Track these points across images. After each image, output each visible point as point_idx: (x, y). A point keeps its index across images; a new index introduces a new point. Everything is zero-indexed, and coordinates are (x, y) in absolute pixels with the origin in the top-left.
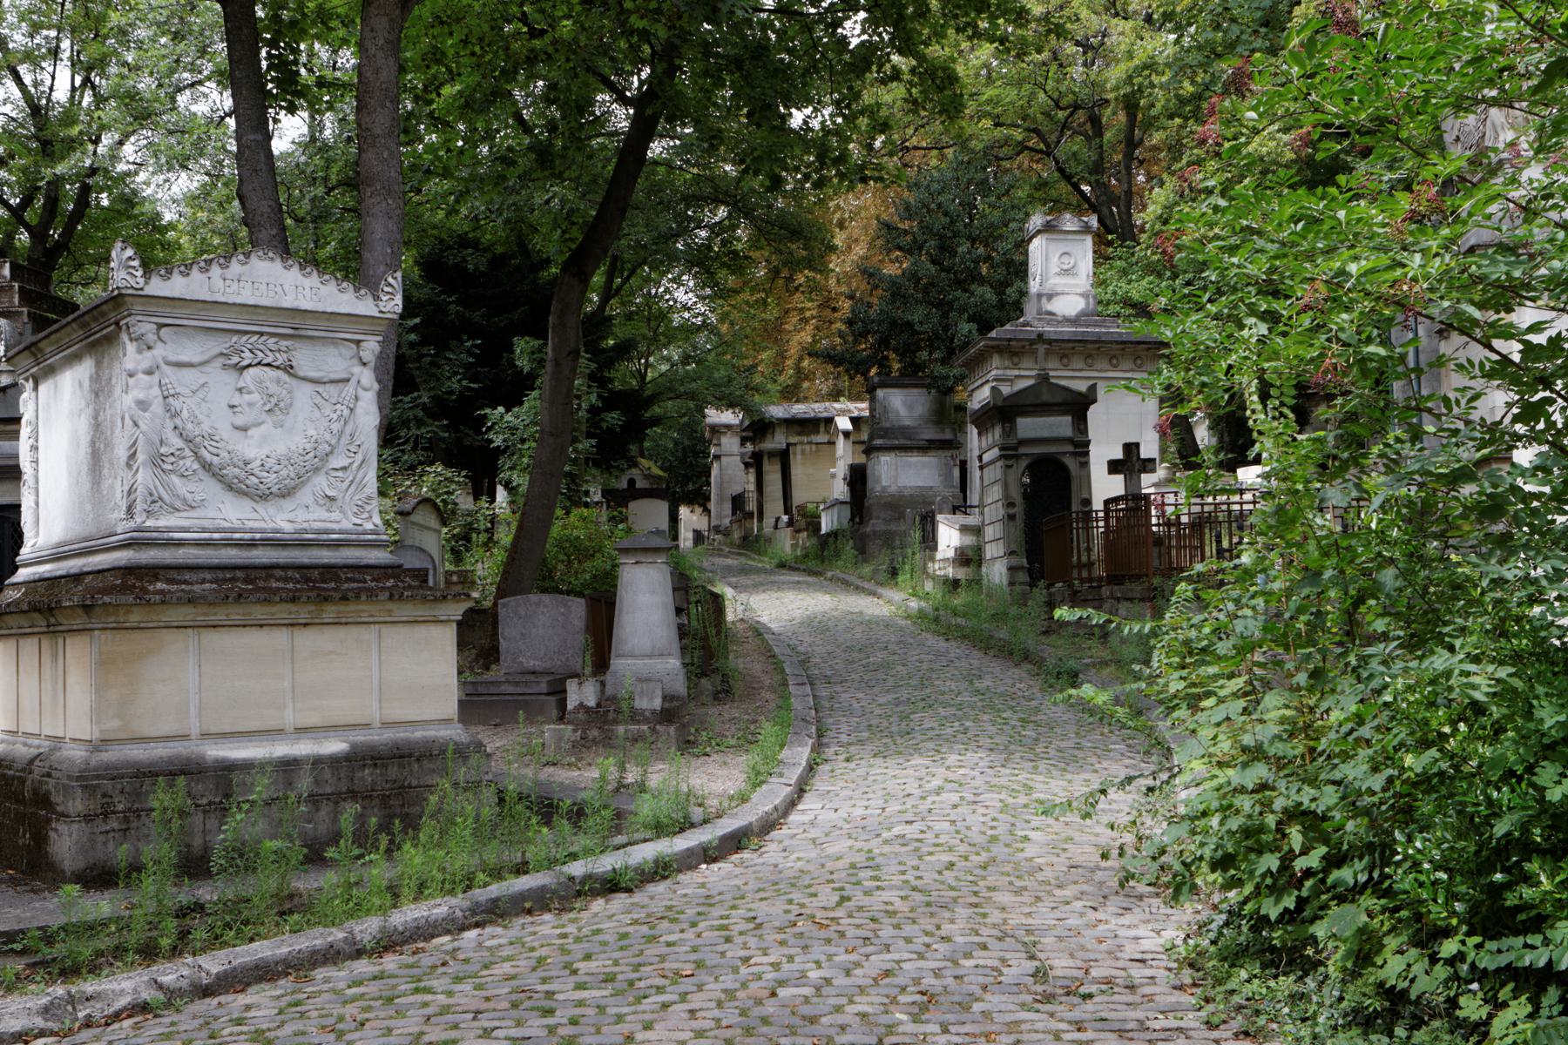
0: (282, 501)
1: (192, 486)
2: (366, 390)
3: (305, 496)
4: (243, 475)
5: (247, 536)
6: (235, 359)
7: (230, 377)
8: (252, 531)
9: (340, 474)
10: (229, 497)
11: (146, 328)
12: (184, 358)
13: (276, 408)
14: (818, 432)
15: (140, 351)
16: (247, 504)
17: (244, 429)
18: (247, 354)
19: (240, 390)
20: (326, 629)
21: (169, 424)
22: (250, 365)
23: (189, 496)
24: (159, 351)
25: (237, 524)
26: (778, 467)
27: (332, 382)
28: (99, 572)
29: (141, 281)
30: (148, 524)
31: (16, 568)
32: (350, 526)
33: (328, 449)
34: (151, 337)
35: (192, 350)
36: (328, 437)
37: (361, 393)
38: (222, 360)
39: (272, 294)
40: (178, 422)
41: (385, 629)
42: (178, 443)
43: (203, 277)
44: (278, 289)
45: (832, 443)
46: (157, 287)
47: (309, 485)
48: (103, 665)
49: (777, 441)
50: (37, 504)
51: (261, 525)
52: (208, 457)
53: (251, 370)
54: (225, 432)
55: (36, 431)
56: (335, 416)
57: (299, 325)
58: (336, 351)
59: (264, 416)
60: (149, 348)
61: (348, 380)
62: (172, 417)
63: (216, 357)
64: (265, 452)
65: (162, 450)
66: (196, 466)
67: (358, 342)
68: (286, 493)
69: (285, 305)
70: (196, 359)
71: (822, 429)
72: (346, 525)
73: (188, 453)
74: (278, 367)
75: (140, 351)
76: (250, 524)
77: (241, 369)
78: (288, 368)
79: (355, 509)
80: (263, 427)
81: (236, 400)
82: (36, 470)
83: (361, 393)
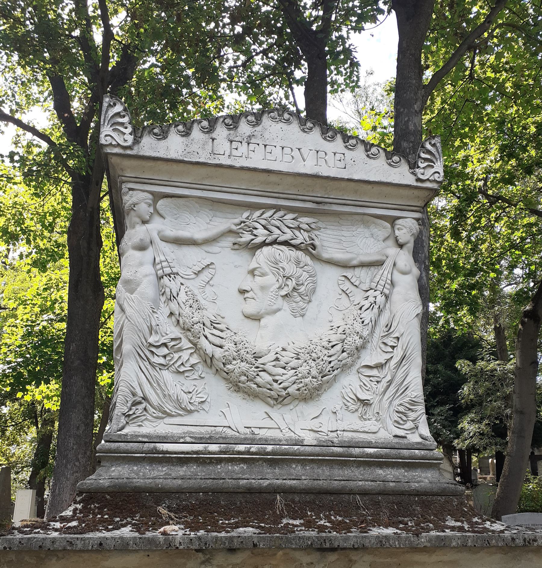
0: (302, 407)
1: (189, 385)
2: (404, 273)
3: (331, 399)
4: (252, 372)
6: (247, 237)
7: (241, 259)
8: (266, 441)
9: (375, 372)
10: (236, 399)
12: (185, 233)
13: (297, 294)
17: (256, 318)
18: (261, 231)
19: (252, 272)
22: (264, 244)
23: (185, 398)
27: (363, 265)
28: (255, 503)
33: (359, 342)
35: (199, 226)
36: (358, 327)
37: (397, 276)
39: (288, 158)
40: (174, 306)
42: (172, 331)
44: (296, 153)
46: (149, 146)
53: (265, 249)
54: (233, 319)
56: (367, 304)
58: (367, 232)
59: (280, 302)
65: (151, 340)
66: (194, 360)
67: (393, 220)
68: (309, 395)
69: (303, 171)
73: (185, 343)
74: (297, 247)
76: (263, 433)
77: (253, 248)
78: (310, 249)
79: (396, 416)
83: (397, 276)
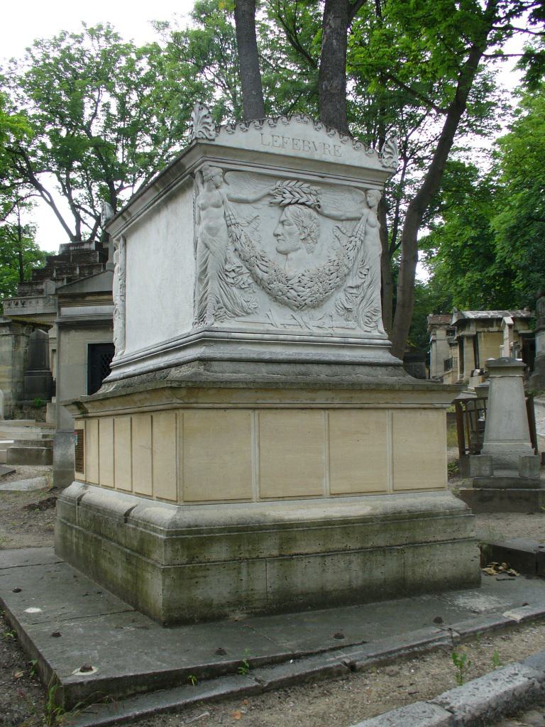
0: (313, 311)
1: (247, 296)
3: (329, 307)
4: (285, 289)
5: (289, 337)
6: (279, 199)
7: (275, 212)
9: (354, 291)
11: (214, 171)
12: (243, 196)
14: (492, 326)
15: (210, 190)
16: (288, 312)
17: (285, 253)
18: (288, 195)
19: (282, 223)
20: (354, 413)
21: (232, 248)
22: (290, 204)
23: (245, 304)
24: (224, 190)
25: (281, 328)
26: (472, 344)
29: (213, 133)
30: (216, 325)
31: (110, 371)
32: (363, 333)
33: (346, 271)
34: (218, 179)
35: (250, 190)
36: (346, 261)
37: (369, 229)
38: (269, 199)
39: (307, 148)
41: (397, 414)
43: (258, 133)
44: (311, 145)
45: (501, 332)
47: (333, 299)
48: (183, 439)
49: (471, 331)
50: (125, 325)
51: (298, 330)
52: (260, 273)
53: (290, 207)
54: (271, 255)
55: (124, 274)
56: (351, 246)
57: (326, 174)
60: (217, 187)
61: (359, 219)
62: (234, 241)
63: (264, 196)
64: (301, 271)
66: (250, 281)
67: (366, 190)
68: (316, 305)
69: (316, 157)
70: (251, 197)
71: (495, 324)
72: (359, 332)
73: (244, 270)
74: (309, 206)
75: (210, 190)
76: (290, 329)
77: (283, 207)
78: (317, 208)
80: (299, 251)
81: (279, 231)
82: (124, 301)
83: (369, 229)
